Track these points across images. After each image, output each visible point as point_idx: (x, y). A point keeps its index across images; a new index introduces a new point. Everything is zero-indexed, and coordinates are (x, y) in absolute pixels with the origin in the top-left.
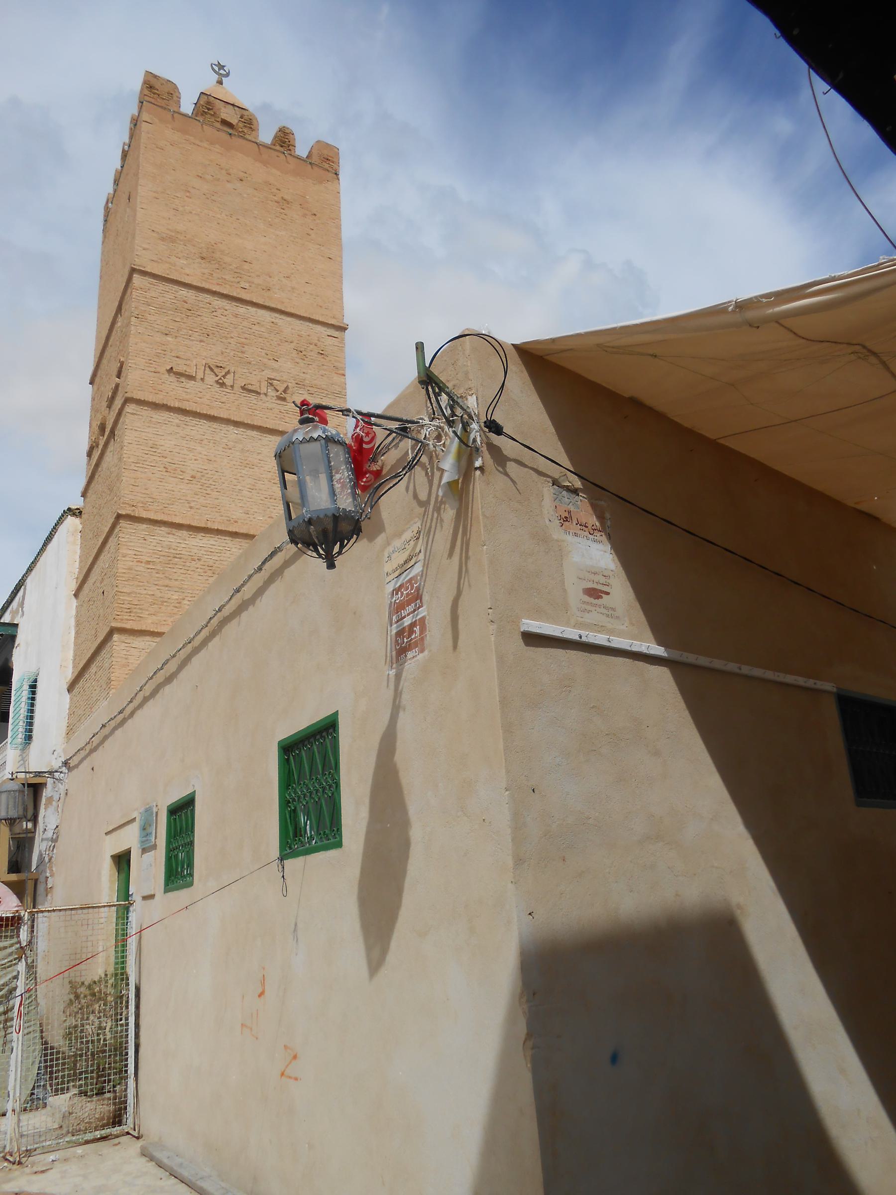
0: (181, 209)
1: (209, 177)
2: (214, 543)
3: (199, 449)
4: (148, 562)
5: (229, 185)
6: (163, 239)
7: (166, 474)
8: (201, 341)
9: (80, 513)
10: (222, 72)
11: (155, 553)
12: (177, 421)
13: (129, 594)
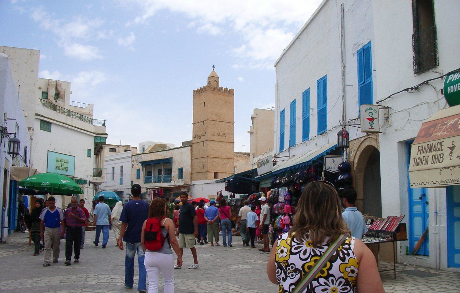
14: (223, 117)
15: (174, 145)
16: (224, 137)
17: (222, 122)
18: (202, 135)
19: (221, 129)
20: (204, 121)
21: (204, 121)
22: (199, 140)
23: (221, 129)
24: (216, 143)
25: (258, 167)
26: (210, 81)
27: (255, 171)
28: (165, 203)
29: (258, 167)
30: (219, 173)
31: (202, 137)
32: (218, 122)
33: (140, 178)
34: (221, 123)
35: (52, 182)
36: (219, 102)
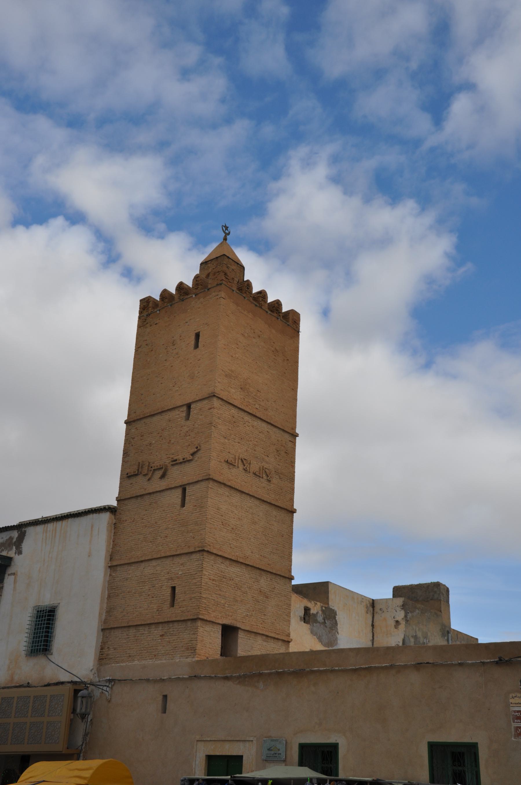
0: (234, 356)
1: (246, 335)
2: (239, 570)
3: (236, 512)
4: (213, 580)
5: (254, 340)
6: (226, 376)
7: (222, 526)
8: (239, 443)
9: (116, 511)
10: (227, 232)
11: (216, 574)
12: (227, 493)
13: (205, 598)
18: (175, 463)
32: (247, 418)
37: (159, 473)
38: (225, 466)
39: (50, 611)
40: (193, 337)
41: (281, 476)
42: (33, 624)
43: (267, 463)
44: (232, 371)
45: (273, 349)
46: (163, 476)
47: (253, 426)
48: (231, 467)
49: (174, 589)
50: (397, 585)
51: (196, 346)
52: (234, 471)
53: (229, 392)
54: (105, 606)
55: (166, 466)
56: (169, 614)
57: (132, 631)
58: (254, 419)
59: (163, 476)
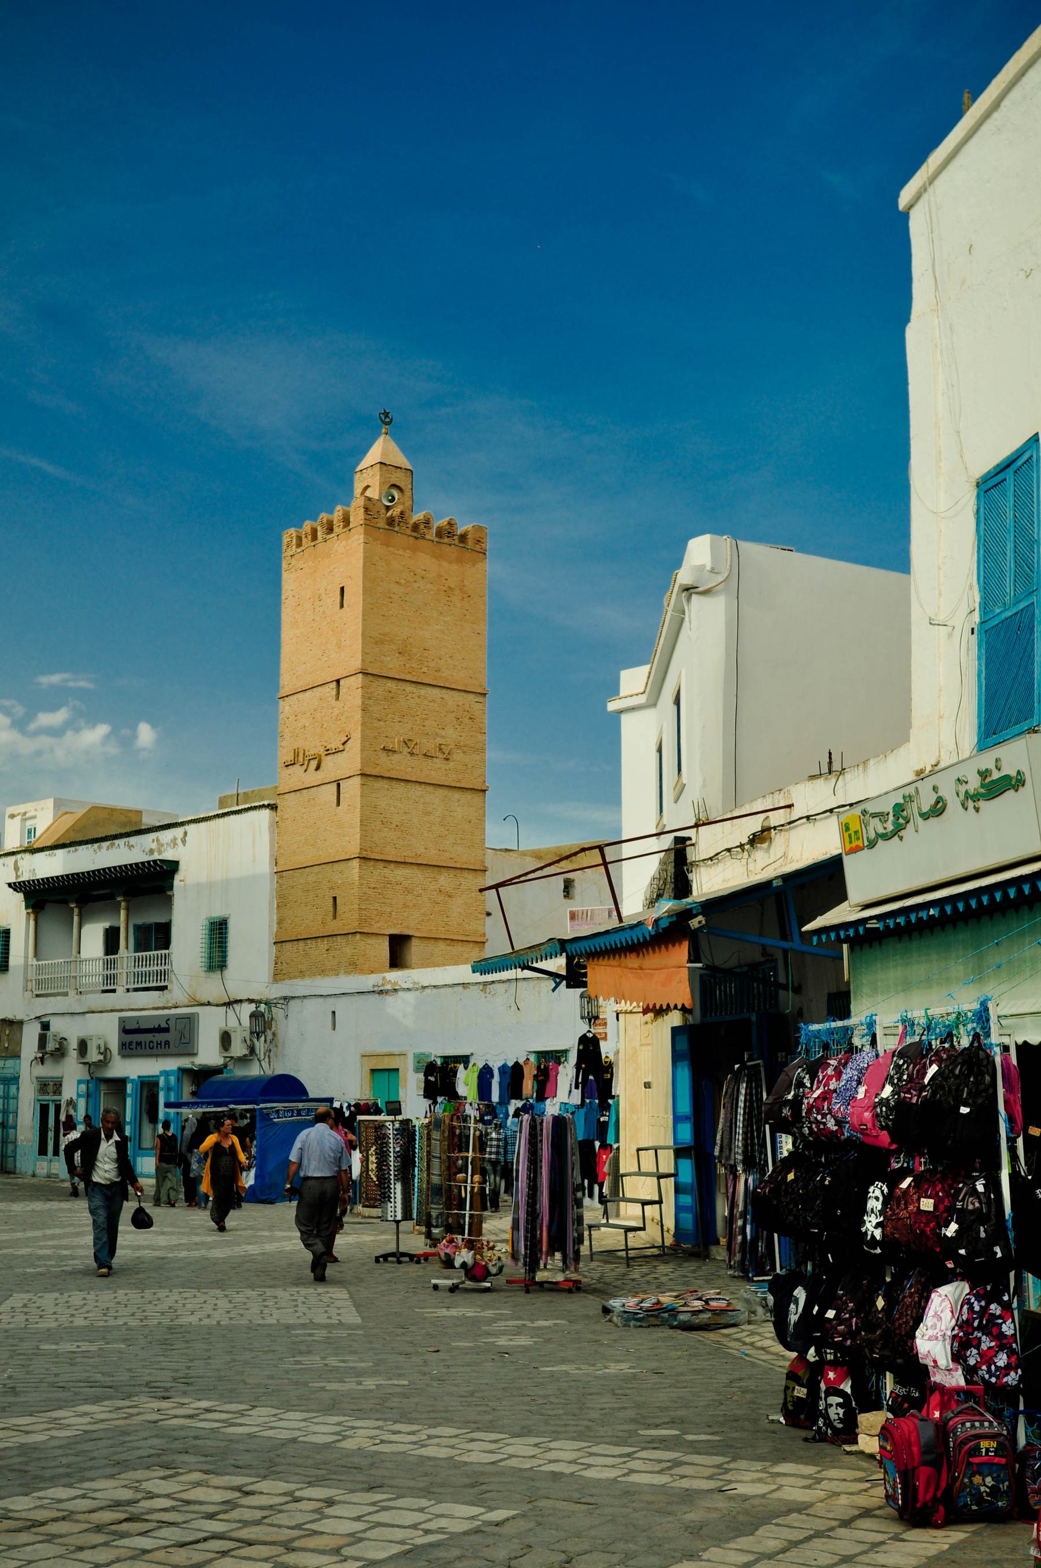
1: (403, 581)
6: (376, 643)
14: (432, 664)
15: (177, 816)
16: (439, 763)
17: (429, 689)
18: (329, 752)
19: (424, 720)
20: (338, 681)
21: (338, 681)
22: (313, 777)
23: (424, 720)
24: (400, 789)
25: (858, 841)
26: (368, 487)
27: (825, 880)
28: (902, 1391)
29: (858, 841)
30: (414, 942)
31: (328, 762)
32: (410, 688)
33: (7, 970)
34: (424, 691)
35: (142, 1074)
36: (416, 585)
37: (314, 764)
38: (383, 755)
39: (221, 924)
40: (338, 592)
41: (465, 749)
42: (207, 941)
43: (443, 737)
44: (385, 635)
45: (444, 588)
46: (318, 768)
47: (419, 697)
48: (390, 753)
49: (335, 898)
50: (902, 751)
51: (342, 606)
52: (395, 757)
53: (382, 662)
54: (275, 917)
55: (320, 756)
56: (334, 927)
57: (301, 944)
58: (420, 686)
59: (318, 768)
